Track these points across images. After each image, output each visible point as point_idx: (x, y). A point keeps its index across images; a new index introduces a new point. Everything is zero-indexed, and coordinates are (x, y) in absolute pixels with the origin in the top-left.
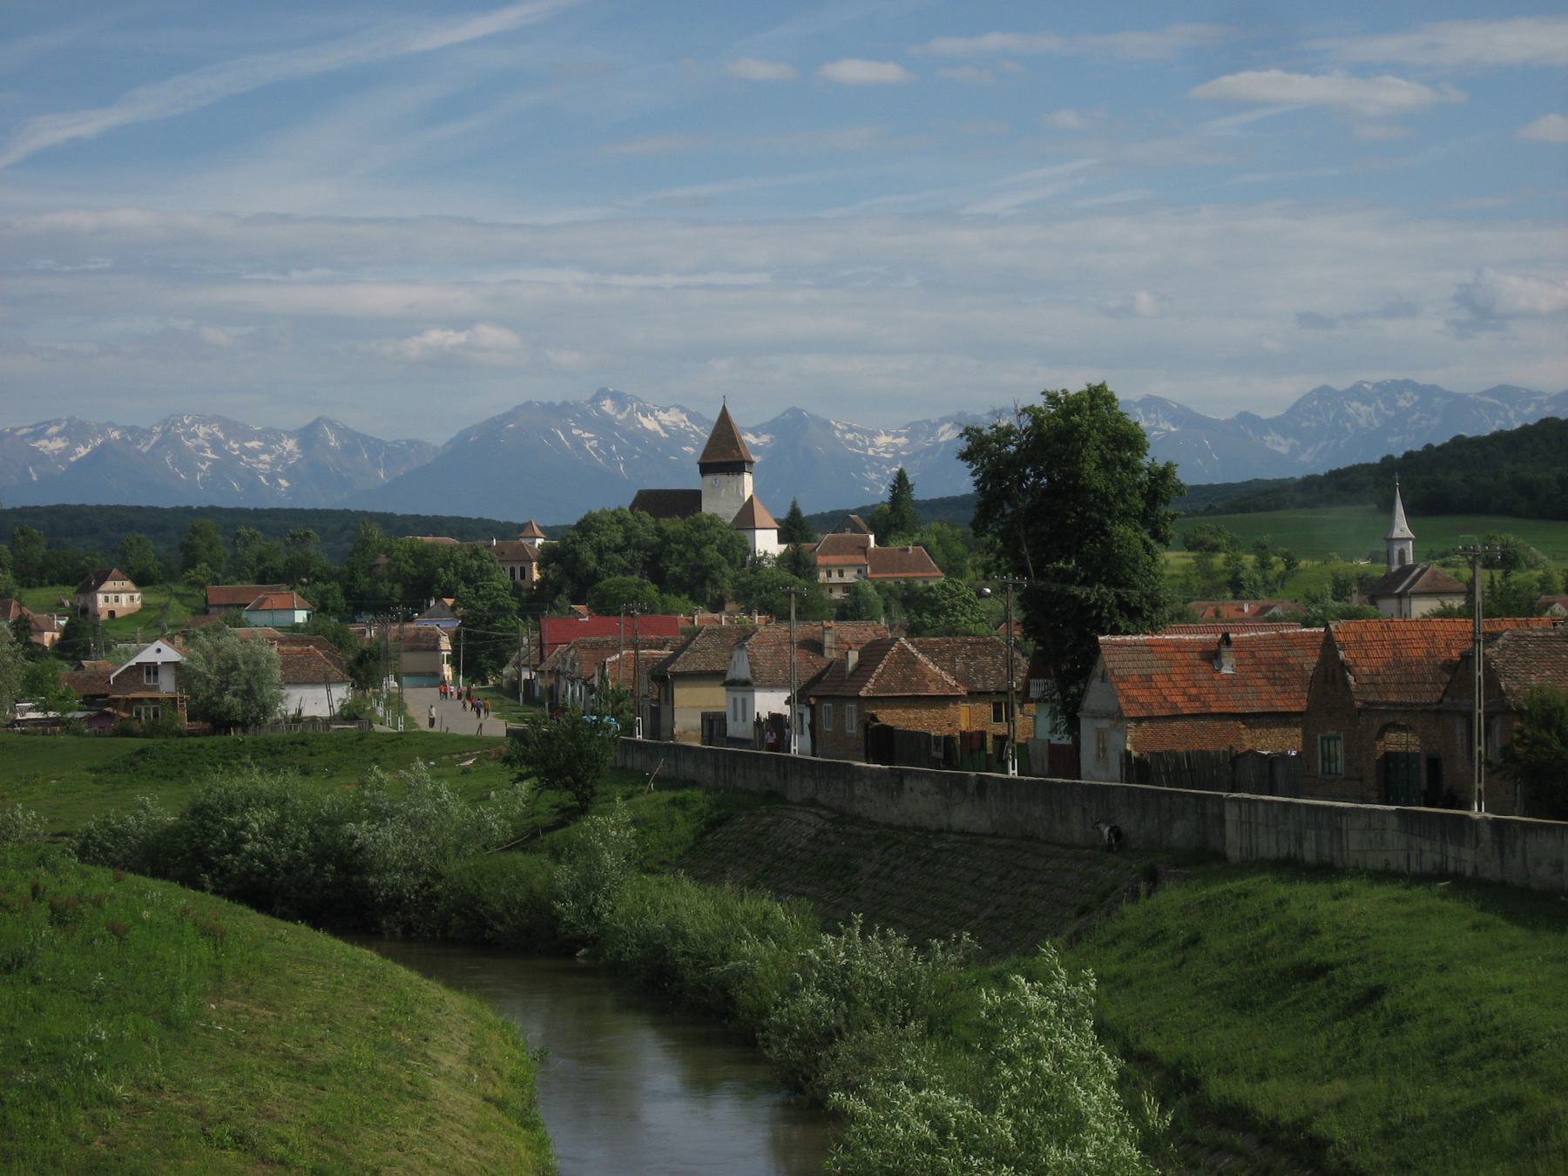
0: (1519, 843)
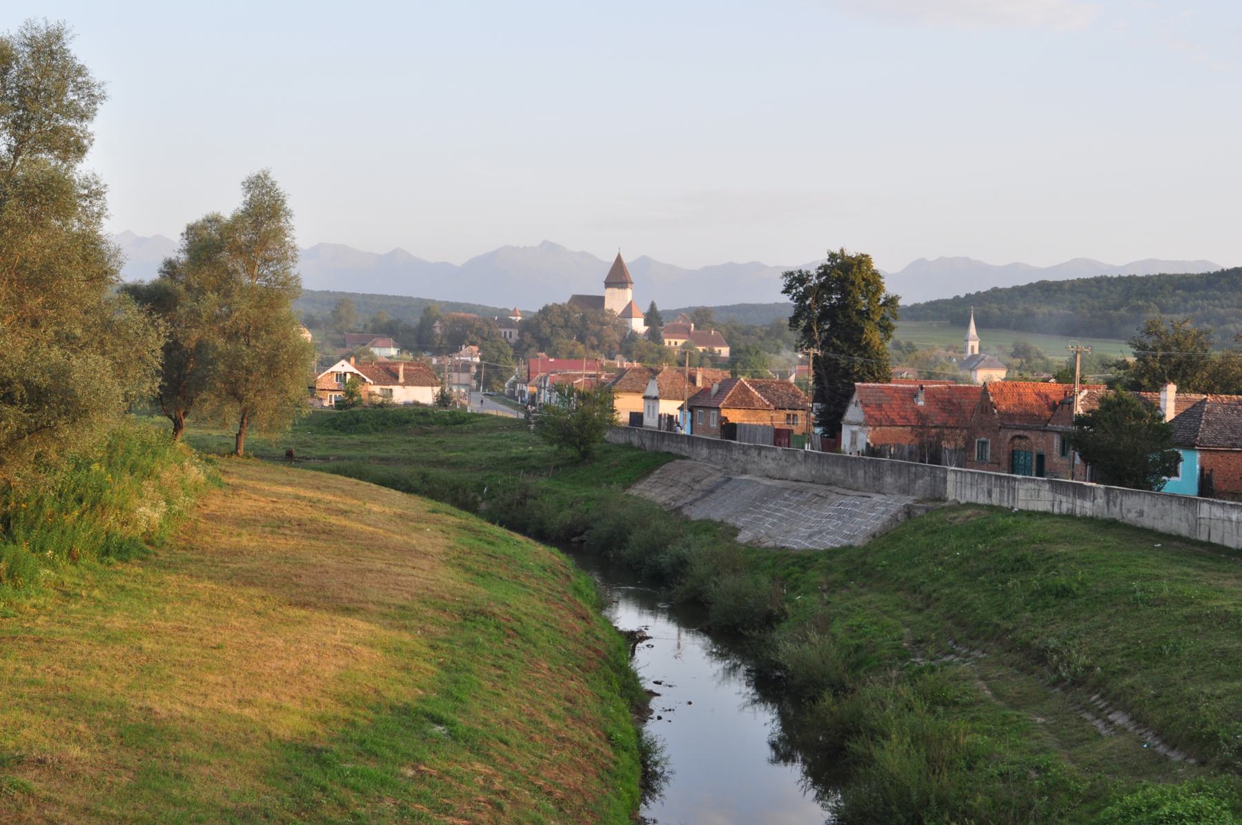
0: (1119, 500)
